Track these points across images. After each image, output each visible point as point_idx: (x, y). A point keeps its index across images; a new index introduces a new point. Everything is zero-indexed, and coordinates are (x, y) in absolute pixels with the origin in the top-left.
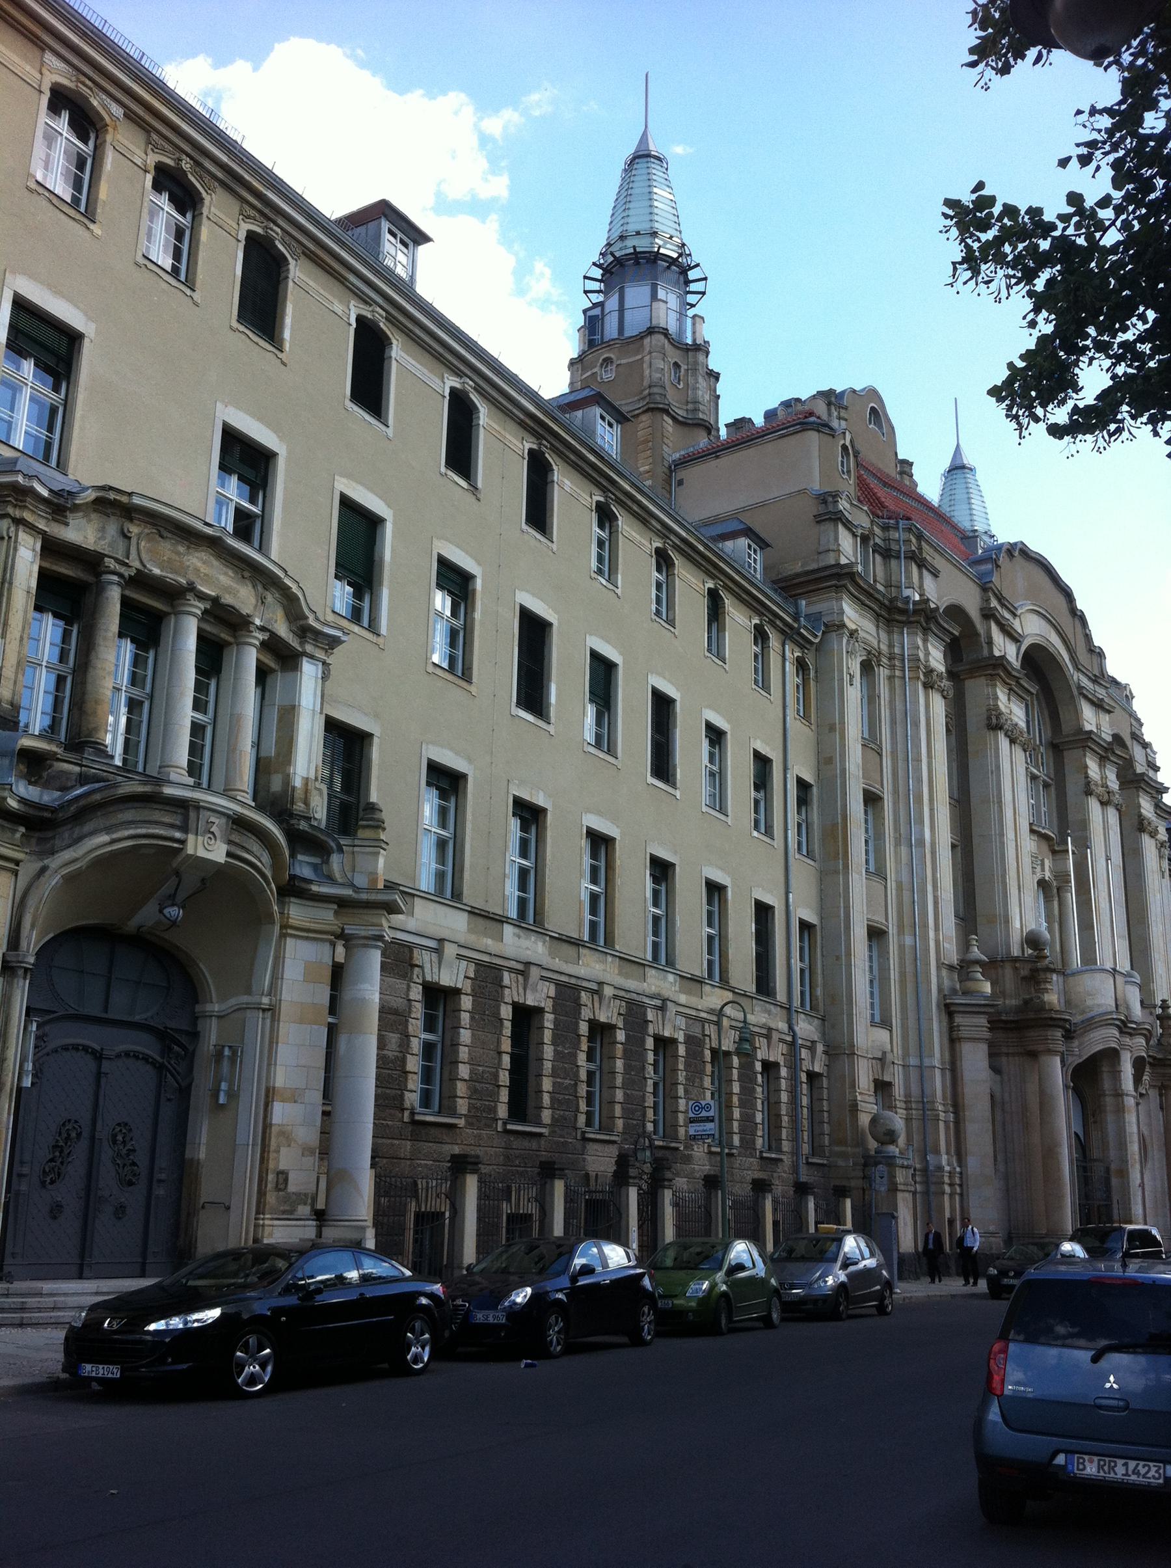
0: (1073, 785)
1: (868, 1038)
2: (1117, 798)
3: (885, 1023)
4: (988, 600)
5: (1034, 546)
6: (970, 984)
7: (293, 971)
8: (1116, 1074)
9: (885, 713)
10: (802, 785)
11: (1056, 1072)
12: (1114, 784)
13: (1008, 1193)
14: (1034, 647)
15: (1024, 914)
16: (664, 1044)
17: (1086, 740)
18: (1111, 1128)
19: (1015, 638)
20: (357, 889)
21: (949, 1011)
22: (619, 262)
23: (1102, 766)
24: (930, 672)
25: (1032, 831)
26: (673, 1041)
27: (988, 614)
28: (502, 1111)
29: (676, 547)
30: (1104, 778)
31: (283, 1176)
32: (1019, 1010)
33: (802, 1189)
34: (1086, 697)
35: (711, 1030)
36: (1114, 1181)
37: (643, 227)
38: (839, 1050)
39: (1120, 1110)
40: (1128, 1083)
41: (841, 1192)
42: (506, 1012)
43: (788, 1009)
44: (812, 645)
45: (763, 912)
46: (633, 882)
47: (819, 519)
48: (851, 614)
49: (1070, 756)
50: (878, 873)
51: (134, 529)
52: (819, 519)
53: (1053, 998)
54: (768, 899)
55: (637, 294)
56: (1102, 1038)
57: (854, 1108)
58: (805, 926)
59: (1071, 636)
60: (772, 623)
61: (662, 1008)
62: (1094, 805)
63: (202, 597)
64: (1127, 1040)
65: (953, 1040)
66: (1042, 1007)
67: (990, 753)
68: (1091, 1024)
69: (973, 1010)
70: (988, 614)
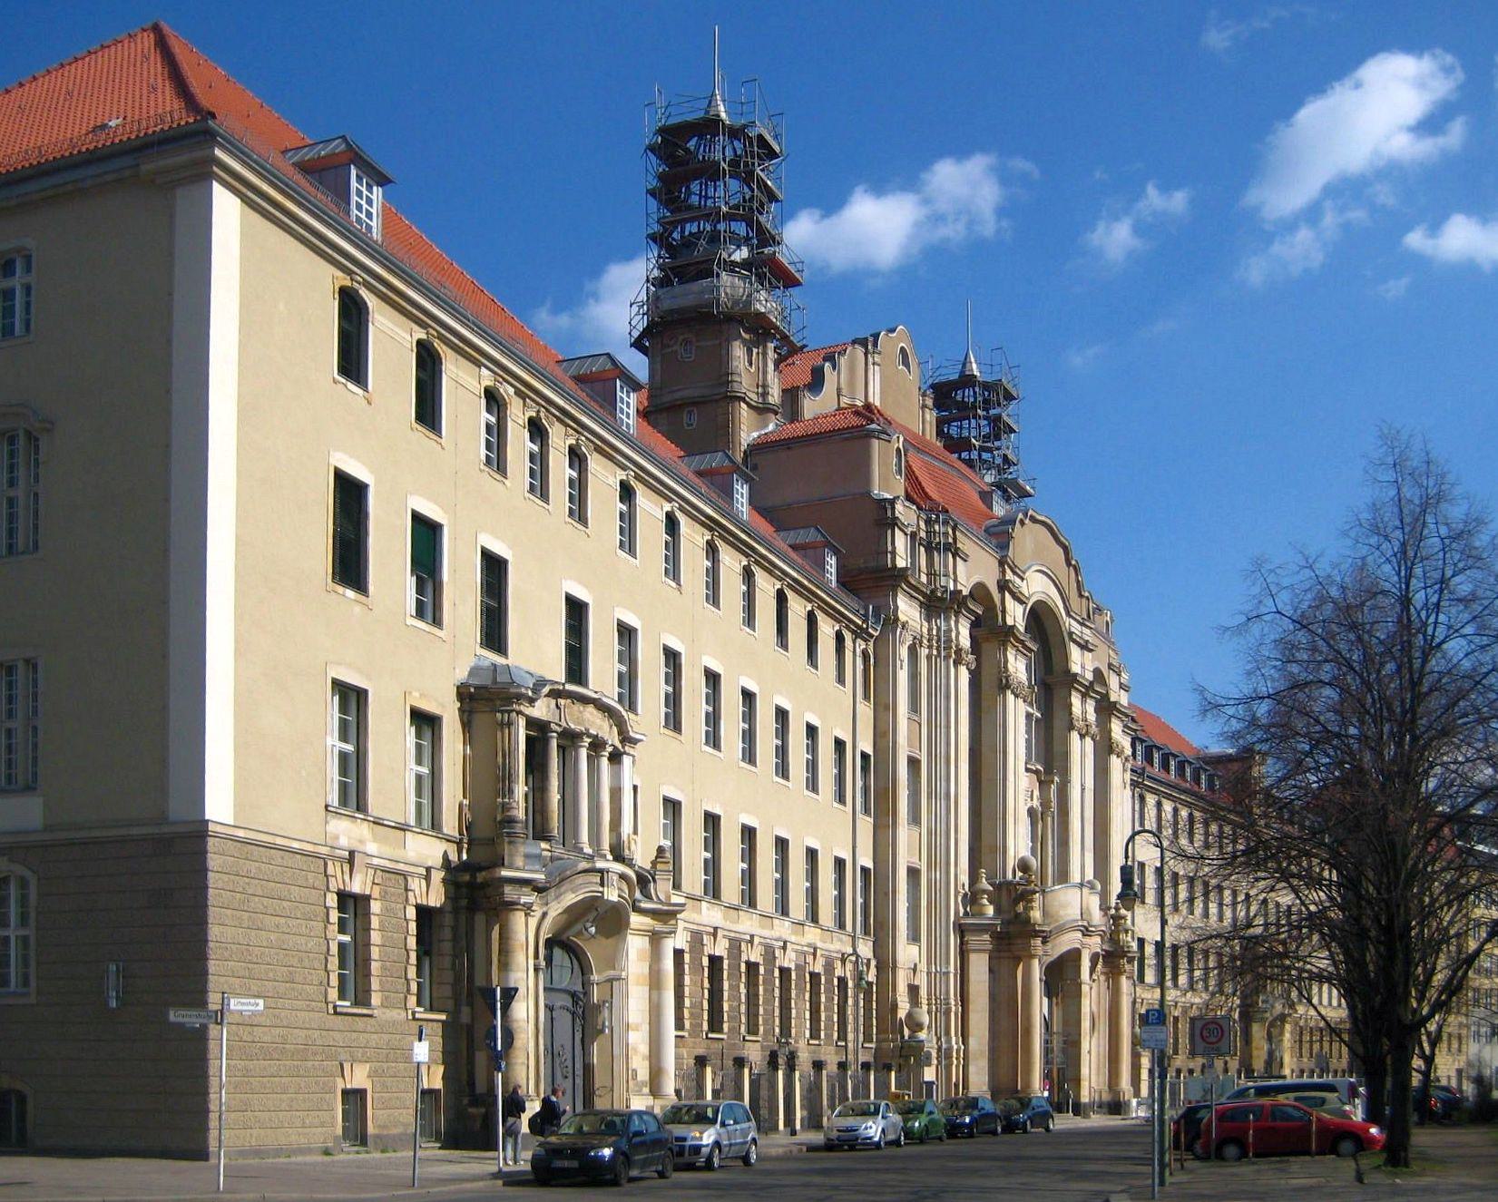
0: (1058, 723)
2: (1094, 729)
4: (1004, 572)
6: (976, 908)
10: (865, 756)
12: (1092, 717)
14: (1039, 602)
15: (1018, 843)
16: (785, 972)
19: (1018, 599)
20: (661, 902)
21: (961, 930)
23: (1083, 702)
24: (959, 651)
25: (1027, 770)
26: (789, 970)
27: (1003, 586)
28: (705, 1027)
29: (789, 586)
30: (1084, 712)
31: (635, 1071)
34: (1075, 642)
35: (810, 959)
41: (888, 1068)
42: (705, 962)
45: (840, 863)
49: (1058, 694)
50: (915, 819)
51: (562, 702)
54: (843, 855)
57: (895, 1007)
59: (1065, 585)
60: (847, 627)
61: (784, 948)
63: (589, 736)
64: (1087, 940)
65: (963, 954)
67: (1000, 709)
69: (980, 929)
70: (1003, 586)
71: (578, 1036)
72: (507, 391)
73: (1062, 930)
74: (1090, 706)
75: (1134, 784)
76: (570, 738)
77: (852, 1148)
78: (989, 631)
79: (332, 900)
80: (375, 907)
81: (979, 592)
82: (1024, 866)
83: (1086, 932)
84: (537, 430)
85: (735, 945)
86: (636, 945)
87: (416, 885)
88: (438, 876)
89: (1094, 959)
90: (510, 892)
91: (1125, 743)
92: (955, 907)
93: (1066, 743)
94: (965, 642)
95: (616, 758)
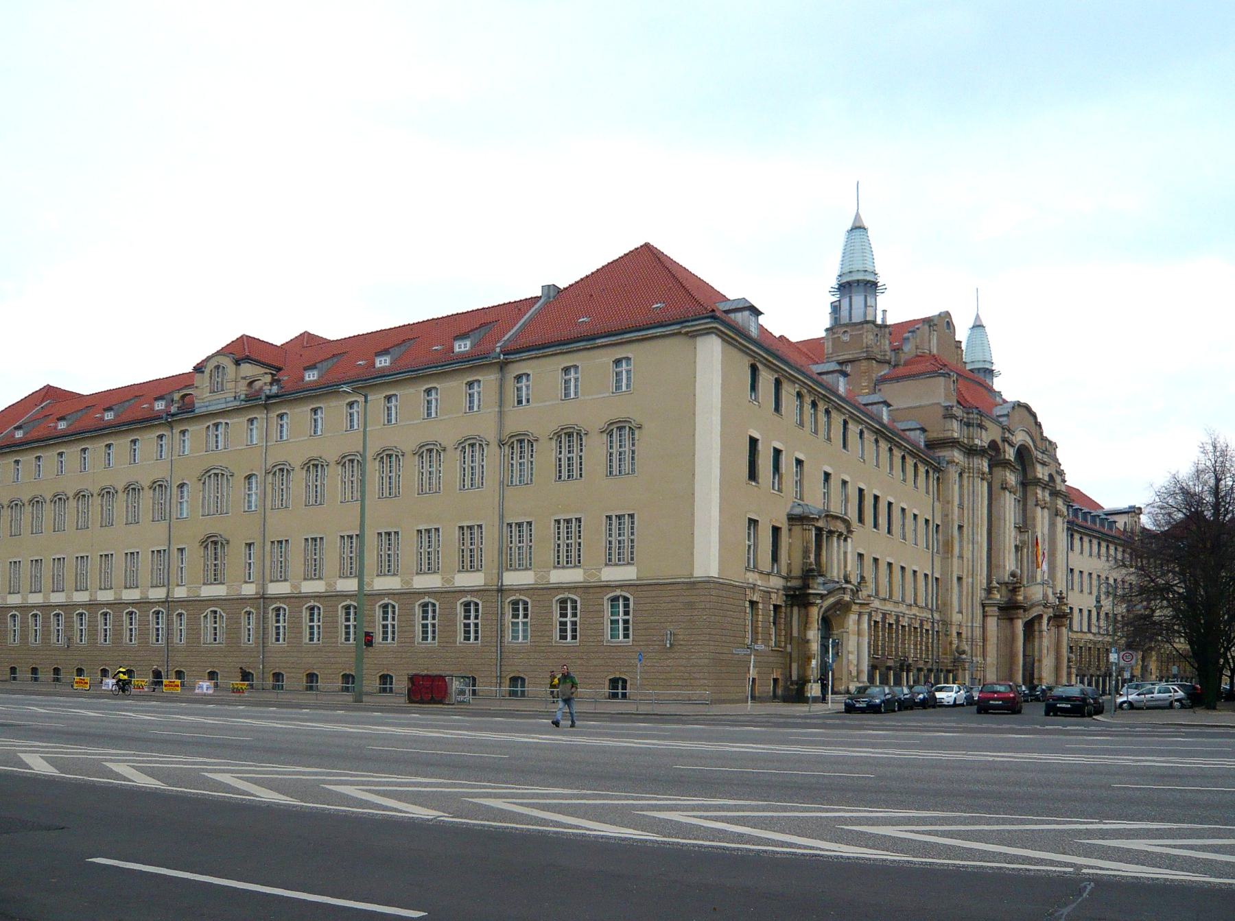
0: (1031, 502)
1: (956, 618)
3: (960, 612)
5: (1022, 401)
7: (851, 622)
8: (1040, 624)
9: (966, 491)
11: (1019, 625)
12: (1048, 498)
13: (807, 616)
15: (1009, 563)
17: (1037, 482)
18: (1036, 644)
19: (1011, 445)
21: (983, 606)
22: (849, 283)
32: (1006, 603)
33: (930, 670)
36: (1036, 664)
37: (861, 268)
38: (946, 623)
39: (1041, 637)
40: (1045, 627)
43: (932, 610)
44: (937, 469)
46: (883, 568)
47: (945, 417)
48: (957, 455)
49: (1030, 488)
52: (945, 417)
53: (1020, 598)
55: (858, 300)
56: (1034, 612)
58: (937, 579)
62: (1039, 509)
65: (985, 616)
66: (1016, 602)
68: (1033, 606)
71: (379, 381)
72: (804, 391)
73: (1033, 606)
74: (1047, 494)
75: (1068, 529)
76: (831, 533)
77: (934, 707)
78: (997, 461)
79: (747, 604)
80: (760, 606)
81: (993, 445)
82: (1013, 575)
83: (1045, 606)
84: (814, 405)
85: (884, 615)
86: (853, 618)
87: (774, 596)
88: (781, 592)
89: (1049, 619)
90: (812, 600)
91: (1064, 509)
92: (980, 594)
93: (1034, 512)
94: (986, 469)
95: (845, 540)
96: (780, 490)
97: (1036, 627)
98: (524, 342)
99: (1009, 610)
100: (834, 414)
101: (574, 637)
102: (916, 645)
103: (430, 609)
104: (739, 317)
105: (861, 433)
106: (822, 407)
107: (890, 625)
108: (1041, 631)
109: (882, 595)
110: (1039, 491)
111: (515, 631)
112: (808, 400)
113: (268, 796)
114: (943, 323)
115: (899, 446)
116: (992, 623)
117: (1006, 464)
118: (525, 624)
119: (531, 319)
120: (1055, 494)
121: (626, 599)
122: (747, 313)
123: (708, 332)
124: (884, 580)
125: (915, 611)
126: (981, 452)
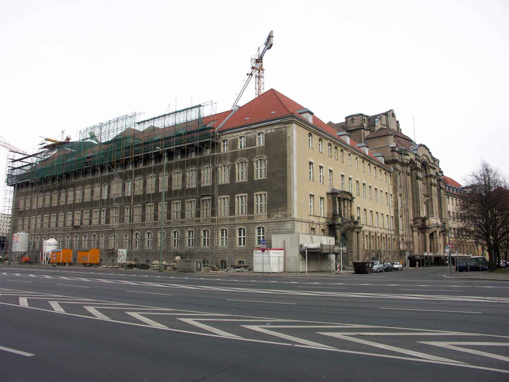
3: (403, 230)
11: (427, 235)
18: (435, 242)
47: (392, 151)
62: (433, 187)
74: (436, 180)
85: (370, 232)
87: (322, 226)
89: (440, 233)
96: (323, 183)
97: (435, 236)
98: (229, 126)
99: (423, 229)
100: (345, 151)
101: (244, 244)
102: (384, 245)
103: (261, 230)
104: (304, 116)
105: (357, 158)
106: (339, 149)
107: (373, 236)
108: (436, 238)
109: (368, 224)
110: (432, 180)
111: (222, 242)
112: (333, 146)
113: (100, 316)
114: (390, 114)
115: (373, 164)
116: (415, 234)
117: (417, 169)
118: (226, 239)
119: (229, 119)
120: (439, 180)
121: (244, 229)
122: (308, 114)
123: (291, 122)
124: (369, 218)
125: (383, 230)
126: (407, 165)
